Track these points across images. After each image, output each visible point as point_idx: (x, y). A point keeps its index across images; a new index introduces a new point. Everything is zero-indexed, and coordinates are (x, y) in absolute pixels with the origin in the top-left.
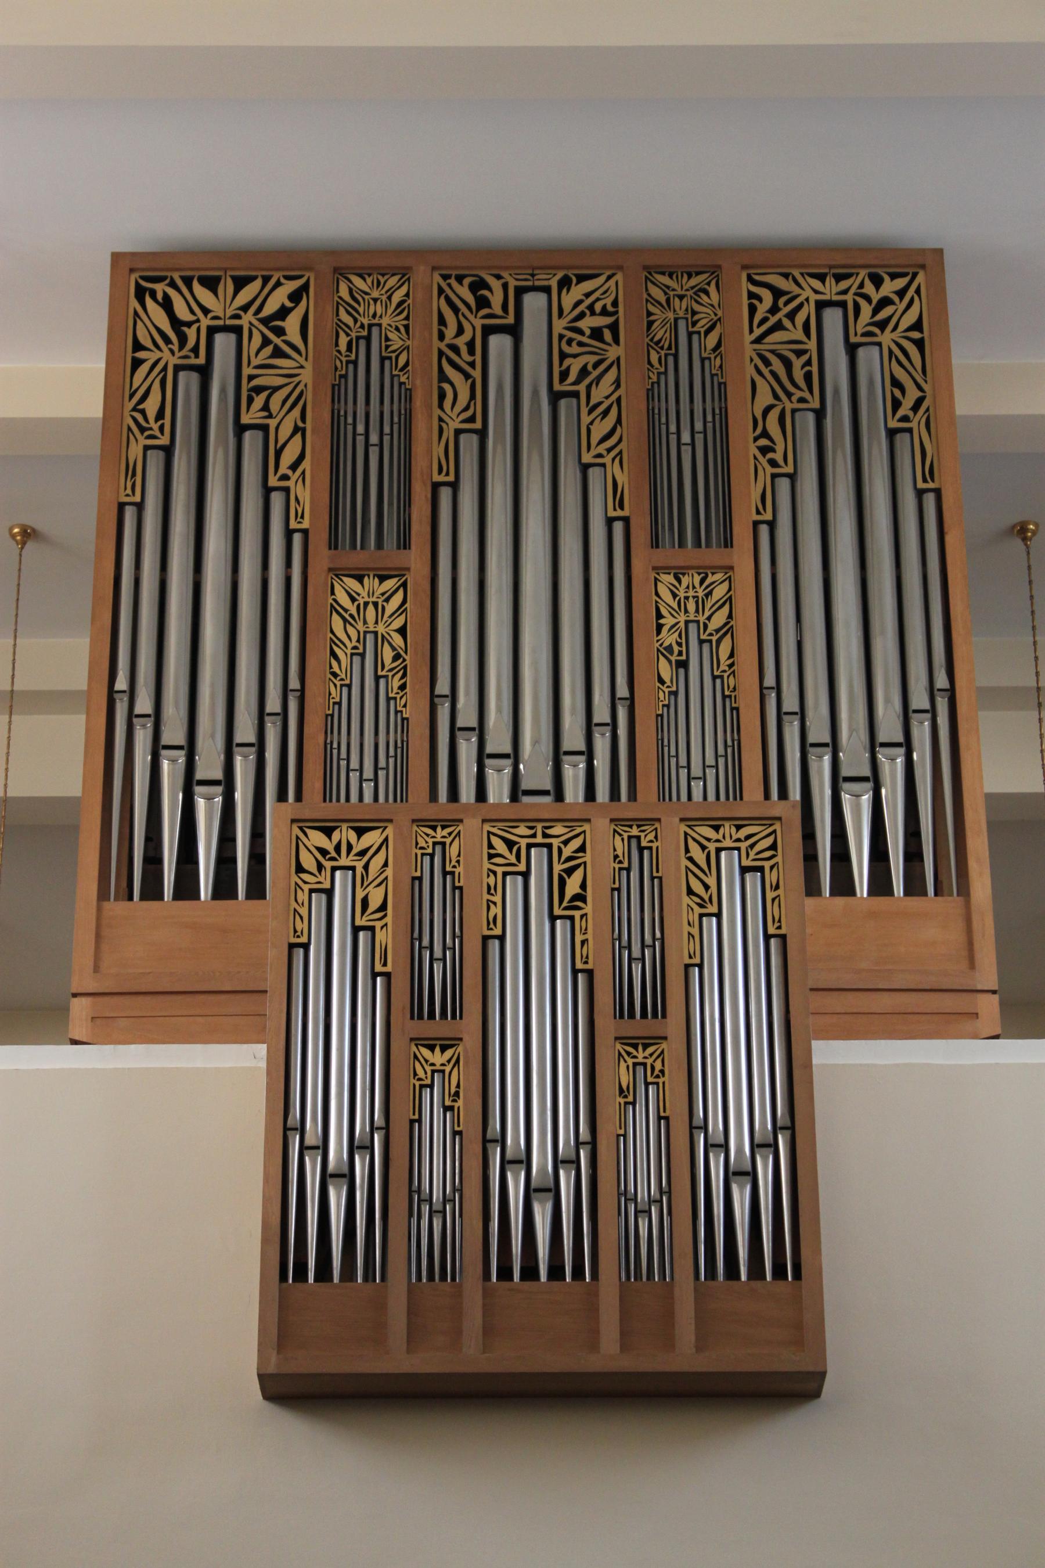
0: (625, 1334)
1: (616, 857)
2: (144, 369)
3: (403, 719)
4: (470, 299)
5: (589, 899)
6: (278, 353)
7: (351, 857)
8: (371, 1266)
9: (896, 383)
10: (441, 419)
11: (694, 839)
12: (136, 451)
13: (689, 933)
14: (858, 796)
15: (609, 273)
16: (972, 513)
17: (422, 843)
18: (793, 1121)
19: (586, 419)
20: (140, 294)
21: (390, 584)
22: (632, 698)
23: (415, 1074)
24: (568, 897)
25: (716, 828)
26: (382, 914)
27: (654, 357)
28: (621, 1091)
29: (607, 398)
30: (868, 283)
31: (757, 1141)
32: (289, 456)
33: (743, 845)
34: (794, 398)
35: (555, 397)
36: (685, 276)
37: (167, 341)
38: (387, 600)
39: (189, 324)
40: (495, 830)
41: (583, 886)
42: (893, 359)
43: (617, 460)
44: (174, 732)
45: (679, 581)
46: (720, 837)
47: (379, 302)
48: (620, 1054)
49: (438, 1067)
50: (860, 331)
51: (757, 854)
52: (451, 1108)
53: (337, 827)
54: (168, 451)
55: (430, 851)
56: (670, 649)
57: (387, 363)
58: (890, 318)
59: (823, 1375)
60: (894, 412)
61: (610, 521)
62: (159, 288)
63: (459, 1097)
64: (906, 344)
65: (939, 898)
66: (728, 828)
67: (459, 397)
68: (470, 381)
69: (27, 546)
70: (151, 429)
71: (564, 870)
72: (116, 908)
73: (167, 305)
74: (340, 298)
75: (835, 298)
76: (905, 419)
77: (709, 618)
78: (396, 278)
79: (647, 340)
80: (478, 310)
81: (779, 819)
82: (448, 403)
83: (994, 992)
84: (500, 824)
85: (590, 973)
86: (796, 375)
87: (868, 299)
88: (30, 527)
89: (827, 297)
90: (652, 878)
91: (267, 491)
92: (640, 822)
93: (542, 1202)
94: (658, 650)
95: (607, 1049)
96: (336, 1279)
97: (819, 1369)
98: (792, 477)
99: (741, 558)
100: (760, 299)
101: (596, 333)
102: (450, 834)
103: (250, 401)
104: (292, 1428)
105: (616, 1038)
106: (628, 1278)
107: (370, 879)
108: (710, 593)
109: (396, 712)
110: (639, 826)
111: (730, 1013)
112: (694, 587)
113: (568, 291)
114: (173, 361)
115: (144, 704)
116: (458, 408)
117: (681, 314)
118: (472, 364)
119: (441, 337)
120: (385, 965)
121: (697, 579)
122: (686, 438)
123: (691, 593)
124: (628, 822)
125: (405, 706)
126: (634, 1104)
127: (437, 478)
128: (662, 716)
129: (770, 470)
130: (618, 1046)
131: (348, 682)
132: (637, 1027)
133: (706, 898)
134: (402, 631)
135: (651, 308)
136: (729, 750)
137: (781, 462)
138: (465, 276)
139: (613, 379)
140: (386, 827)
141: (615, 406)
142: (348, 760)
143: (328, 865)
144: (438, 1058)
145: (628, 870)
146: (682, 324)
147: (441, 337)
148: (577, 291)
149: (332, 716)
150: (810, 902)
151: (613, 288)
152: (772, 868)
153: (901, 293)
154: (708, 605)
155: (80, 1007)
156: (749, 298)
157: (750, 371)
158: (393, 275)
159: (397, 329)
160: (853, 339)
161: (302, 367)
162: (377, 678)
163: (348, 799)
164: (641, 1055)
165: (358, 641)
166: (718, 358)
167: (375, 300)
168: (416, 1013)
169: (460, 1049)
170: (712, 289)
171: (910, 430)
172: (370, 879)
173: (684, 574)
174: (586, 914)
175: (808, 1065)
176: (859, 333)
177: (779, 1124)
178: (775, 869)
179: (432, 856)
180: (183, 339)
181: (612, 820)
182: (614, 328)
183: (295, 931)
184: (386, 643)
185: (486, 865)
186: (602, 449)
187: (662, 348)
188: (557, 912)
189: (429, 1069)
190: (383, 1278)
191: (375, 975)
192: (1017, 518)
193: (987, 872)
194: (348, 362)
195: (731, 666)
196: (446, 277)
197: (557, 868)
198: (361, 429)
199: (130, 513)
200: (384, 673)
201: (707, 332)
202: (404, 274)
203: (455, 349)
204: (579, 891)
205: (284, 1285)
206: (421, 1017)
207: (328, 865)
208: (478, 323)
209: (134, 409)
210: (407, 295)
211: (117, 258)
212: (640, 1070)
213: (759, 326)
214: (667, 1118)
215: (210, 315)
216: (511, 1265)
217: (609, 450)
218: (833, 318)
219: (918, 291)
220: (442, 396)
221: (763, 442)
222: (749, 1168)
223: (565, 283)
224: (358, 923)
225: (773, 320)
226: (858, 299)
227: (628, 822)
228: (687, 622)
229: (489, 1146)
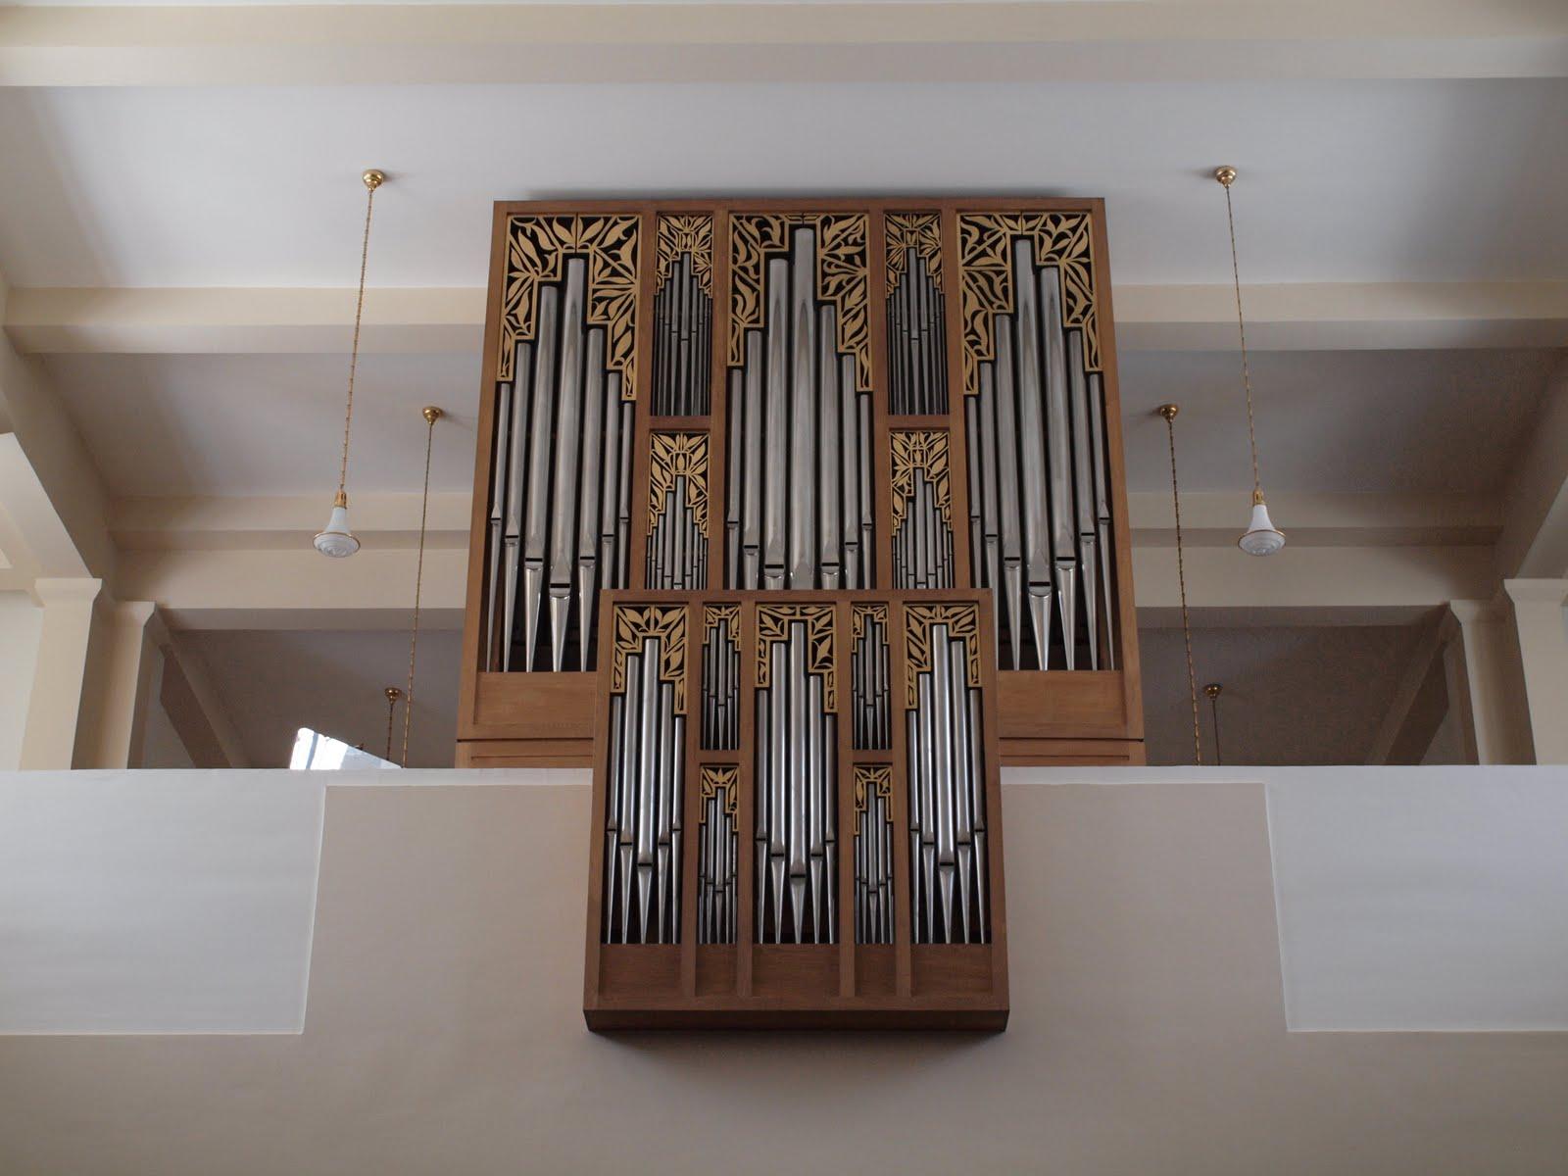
0: (858, 982)
1: (855, 630)
2: (516, 285)
3: (704, 539)
4: (757, 234)
5: (835, 661)
6: (615, 273)
7: (657, 629)
8: (669, 932)
9: (1070, 295)
10: (734, 321)
11: (913, 617)
12: (510, 344)
13: (910, 687)
14: (1041, 596)
15: (859, 215)
16: (1131, 399)
17: (710, 619)
18: (986, 824)
19: (840, 321)
20: (514, 231)
21: (695, 441)
22: (873, 525)
23: (704, 790)
24: (818, 660)
25: (930, 609)
26: (679, 672)
27: (892, 276)
28: (857, 803)
29: (856, 305)
30: (1049, 222)
31: (959, 839)
32: (621, 348)
33: (950, 622)
34: (995, 306)
35: (818, 305)
36: (915, 218)
37: (534, 264)
38: (693, 452)
39: (550, 253)
40: (765, 610)
41: (830, 651)
42: (1068, 278)
43: (864, 351)
44: (535, 550)
45: (909, 439)
46: (933, 616)
47: (689, 237)
48: (857, 776)
49: (721, 785)
50: (1043, 257)
51: (961, 627)
52: (730, 815)
53: (647, 608)
54: (534, 344)
55: (716, 625)
56: (902, 488)
57: (695, 280)
58: (1065, 248)
59: (1007, 1013)
60: (1069, 315)
61: (858, 395)
62: (529, 226)
63: (736, 807)
64: (1078, 267)
65: (1100, 671)
66: (938, 609)
67: (745, 295)
68: (755, 294)
69: (435, 423)
70: (521, 328)
71: (815, 640)
72: (490, 677)
73: (534, 239)
74: (661, 233)
75: (1025, 233)
76: (1077, 321)
77: (931, 466)
78: (702, 219)
79: (887, 264)
80: (762, 242)
81: (977, 602)
82: (739, 310)
83: (1141, 740)
84: (769, 606)
85: (835, 716)
86: (997, 290)
87: (1049, 234)
88: (437, 409)
89: (1020, 233)
90: (882, 646)
91: (605, 373)
92: (873, 604)
93: (797, 885)
94: (894, 489)
95: (847, 772)
96: (643, 941)
97: (1004, 1008)
98: (994, 363)
99: (955, 422)
100: (970, 234)
101: (849, 259)
102: (731, 613)
103: (594, 308)
104: (615, 1061)
105: (854, 764)
106: (862, 941)
107: (672, 645)
108: (932, 447)
109: (699, 534)
110: (872, 607)
111: (940, 742)
112: (920, 443)
113: (829, 228)
114: (538, 279)
115: (513, 529)
116: (747, 312)
117: (912, 245)
118: (757, 281)
119: (735, 261)
120: (682, 709)
121: (922, 437)
122: (915, 334)
123: (918, 447)
124: (864, 604)
125: (705, 530)
126: (867, 813)
127: (731, 363)
128: (896, 537)
129: (977, 358)
130: (856, 770)
131: (663, 512)
132: (870, 756)
133: (923, 660)
134: (704, 475)
135: (889, 240)
136: (946, 563)
137: (985, 352)
138: (753, 217)
139: (860, 293)
140: (683, 608)
141: (862, 313)
142: (663, 569)
143: (640, 635)
144: (721, 778)
145: (864, 639)
146: (912, 251)
147: (735, 261)
148: (835, 228)
149: (652, 537)
150: (1004, 675)
151: (862, 226)
152: (971, 638)
153: (1074, 230)
154: (930, 457)
155: (463, 750)
156: (962, 233)
157: (962, 286)
158: (700, 217)
159: (702, 255)
160: (1038, 263)
161: (632, 283)
162: (685, 509)
163: (656, 587)
164: (872, 777)
165: (671, 482)
166: (939, 277)
167: (687, 235)
168: (705, 744)
169: (737, 772)
170: (935, 227)
171: (1080, 329)
172: (672, 645)
173: (912, 434)
174: (832, 672)
175: (997, 783)
176: (1043, 257)
177: (976, 827)
178: (974, 639)
179: (718, 629)
180: (545, 264)
181: (852, 603)
182: (862, 254)
183: (615, 684)
184: (692, 484)
185: (758, 635)
186: (852, 342)
187: (897, 269)
188: (811, 670)
189: (714, 786)
190: (679, 940)
191: (674, 717)
192: (1162, 402)
193: (1136, 653)
194: (666, 280)
195: (947, 501)
196: (738, 218)
197: (811, 638)
198: (675, 328)
199: (504, 389)
200: (690, 506)
201: (931, 257)
202: (708, 215)
203: (745, 270)
204: (827, 655)
205: (605, 945)
206: (708, 747)
207: (640, 635)
208: (762, 251)
209: (509, 314)
210: (710, 231)
211: (497, 205)
212: (871, 787)
213: (969, 253)
214: (891, 823)
215: (565, 246)
216: (772, 931)
217: (858, 343)
218: (1023, 248)
219: (1086, 229)
220: (735, 302)
221: (972, 337)
222: (952, 860)
223: (826, 222)
224: (662, 678)
225: (980, 249)
226: (1042, 234)
227: (864, 604)
228: (915, 469)
229: (759, 843)
